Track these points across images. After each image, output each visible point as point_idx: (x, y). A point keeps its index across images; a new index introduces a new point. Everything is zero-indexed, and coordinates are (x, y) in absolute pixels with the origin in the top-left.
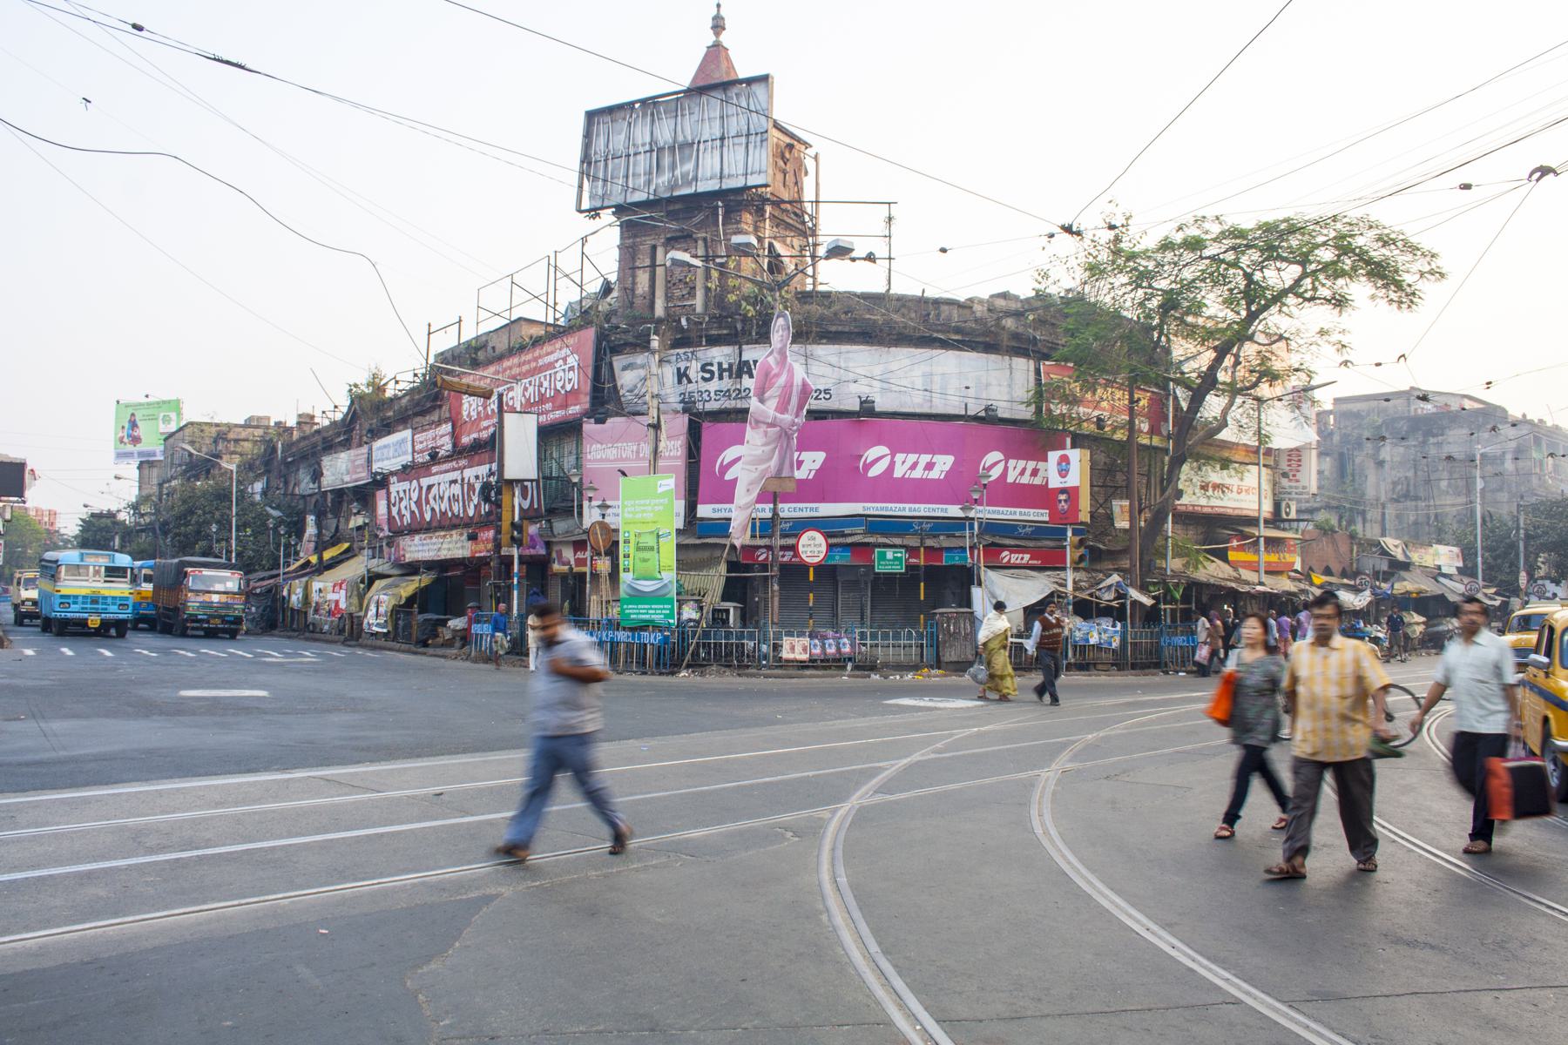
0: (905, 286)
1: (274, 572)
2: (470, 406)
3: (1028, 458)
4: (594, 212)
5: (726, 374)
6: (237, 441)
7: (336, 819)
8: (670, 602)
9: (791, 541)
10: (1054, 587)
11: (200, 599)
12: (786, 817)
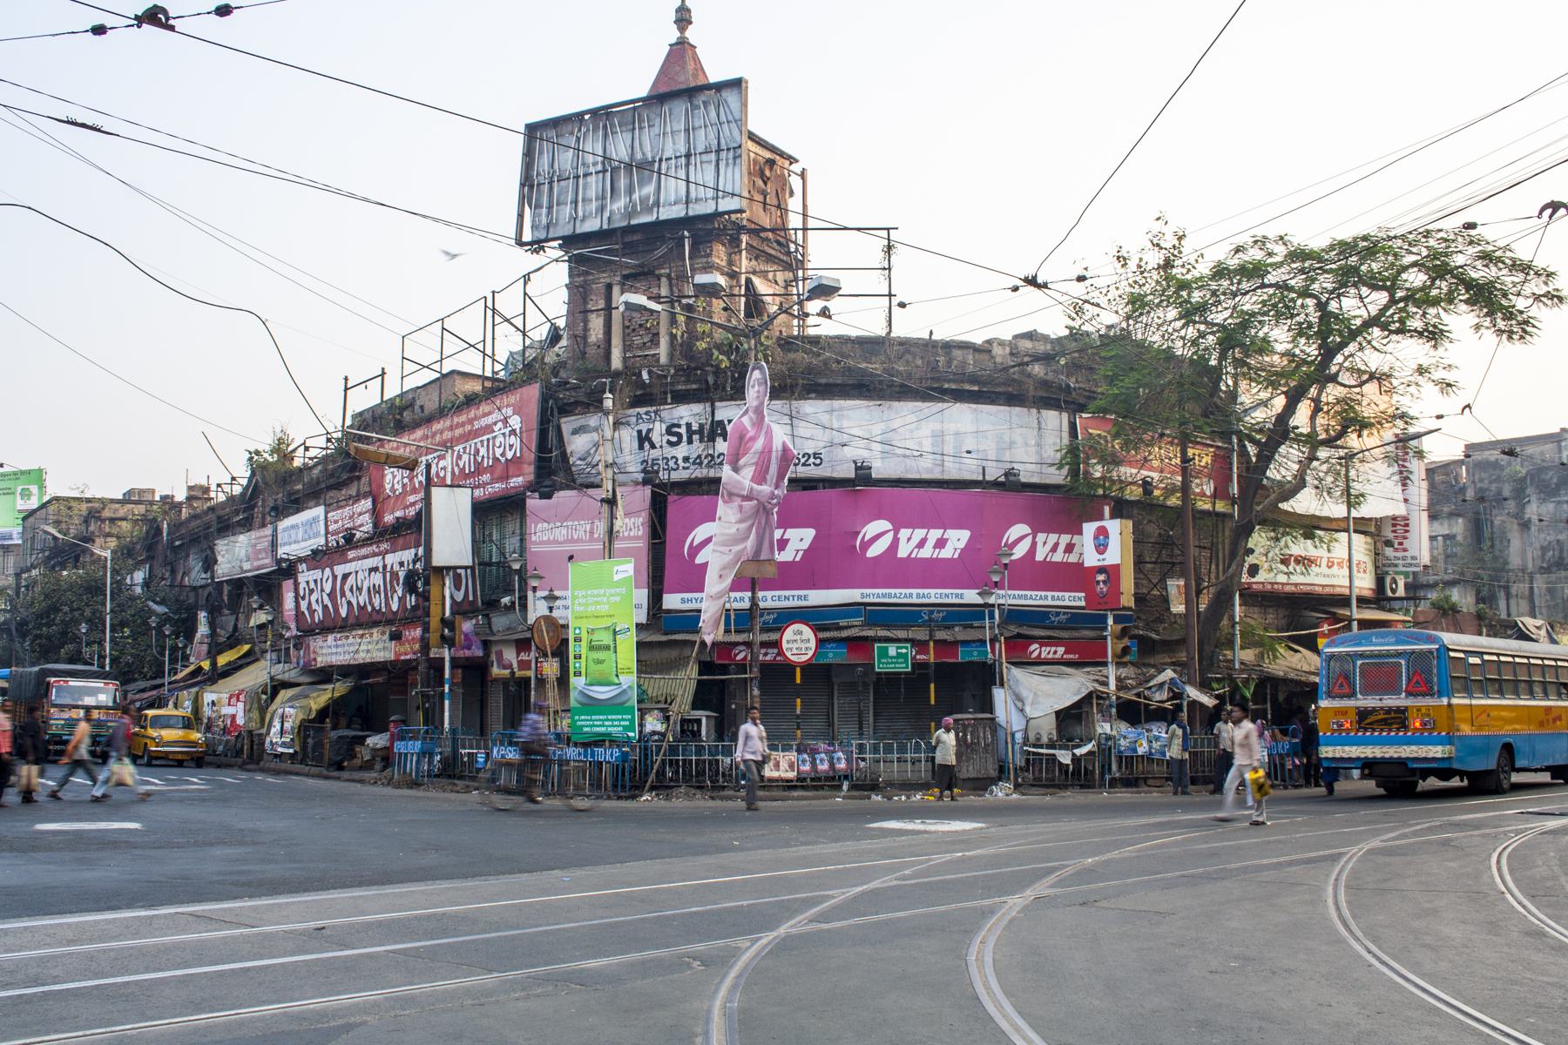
0: (908, 327)
1: (158, 681)
2: (393, 479)
3: (1060, 532)
4: (537, 246)
5: (696, 437)
6: (112, 520)
7: (200, 953)
8: (630, 711)
9: (774, 636)
10: (1091, 686)
11: (66, 715)
12: (700, 947)
